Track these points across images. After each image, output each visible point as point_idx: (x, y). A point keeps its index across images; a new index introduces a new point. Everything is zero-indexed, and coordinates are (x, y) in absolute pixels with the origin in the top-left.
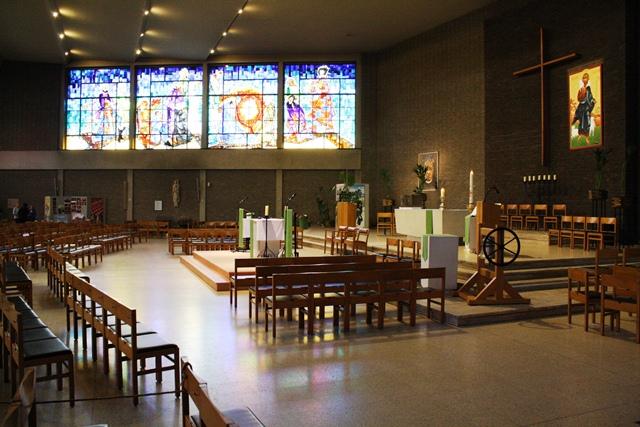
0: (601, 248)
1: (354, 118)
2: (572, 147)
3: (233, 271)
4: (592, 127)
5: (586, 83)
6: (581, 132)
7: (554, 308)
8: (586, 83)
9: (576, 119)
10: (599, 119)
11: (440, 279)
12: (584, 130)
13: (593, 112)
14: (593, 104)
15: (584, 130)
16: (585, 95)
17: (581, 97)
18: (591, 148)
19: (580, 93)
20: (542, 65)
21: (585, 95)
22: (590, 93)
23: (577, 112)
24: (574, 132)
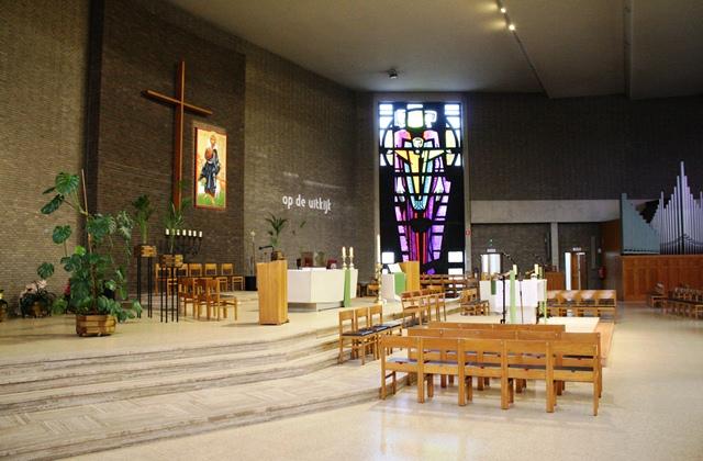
0: (211, 113)
1: (79, 115)
2: (198, 204)
3: (338, 324)
4: (218, 190)
5: (213, 145)
6: (207, 190)
7: (241, 191)
8: (213, 145)
9: (202, 176)
10: (224, 184)
11: (617, 201)
12: (210, 190)
13: (219, 175)
14: (219, 168)
15: (210, 190)
16: (211, 155)
17: (208, 157)
18: (216, 209)
19: (207, 152)
20: (182, 103)
21: (211, 155)
22: (216, 156)
23: (204, 169)
24: (201, 189)
